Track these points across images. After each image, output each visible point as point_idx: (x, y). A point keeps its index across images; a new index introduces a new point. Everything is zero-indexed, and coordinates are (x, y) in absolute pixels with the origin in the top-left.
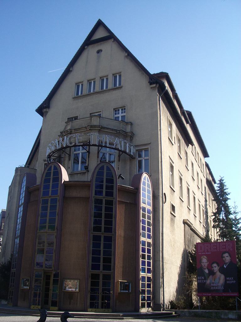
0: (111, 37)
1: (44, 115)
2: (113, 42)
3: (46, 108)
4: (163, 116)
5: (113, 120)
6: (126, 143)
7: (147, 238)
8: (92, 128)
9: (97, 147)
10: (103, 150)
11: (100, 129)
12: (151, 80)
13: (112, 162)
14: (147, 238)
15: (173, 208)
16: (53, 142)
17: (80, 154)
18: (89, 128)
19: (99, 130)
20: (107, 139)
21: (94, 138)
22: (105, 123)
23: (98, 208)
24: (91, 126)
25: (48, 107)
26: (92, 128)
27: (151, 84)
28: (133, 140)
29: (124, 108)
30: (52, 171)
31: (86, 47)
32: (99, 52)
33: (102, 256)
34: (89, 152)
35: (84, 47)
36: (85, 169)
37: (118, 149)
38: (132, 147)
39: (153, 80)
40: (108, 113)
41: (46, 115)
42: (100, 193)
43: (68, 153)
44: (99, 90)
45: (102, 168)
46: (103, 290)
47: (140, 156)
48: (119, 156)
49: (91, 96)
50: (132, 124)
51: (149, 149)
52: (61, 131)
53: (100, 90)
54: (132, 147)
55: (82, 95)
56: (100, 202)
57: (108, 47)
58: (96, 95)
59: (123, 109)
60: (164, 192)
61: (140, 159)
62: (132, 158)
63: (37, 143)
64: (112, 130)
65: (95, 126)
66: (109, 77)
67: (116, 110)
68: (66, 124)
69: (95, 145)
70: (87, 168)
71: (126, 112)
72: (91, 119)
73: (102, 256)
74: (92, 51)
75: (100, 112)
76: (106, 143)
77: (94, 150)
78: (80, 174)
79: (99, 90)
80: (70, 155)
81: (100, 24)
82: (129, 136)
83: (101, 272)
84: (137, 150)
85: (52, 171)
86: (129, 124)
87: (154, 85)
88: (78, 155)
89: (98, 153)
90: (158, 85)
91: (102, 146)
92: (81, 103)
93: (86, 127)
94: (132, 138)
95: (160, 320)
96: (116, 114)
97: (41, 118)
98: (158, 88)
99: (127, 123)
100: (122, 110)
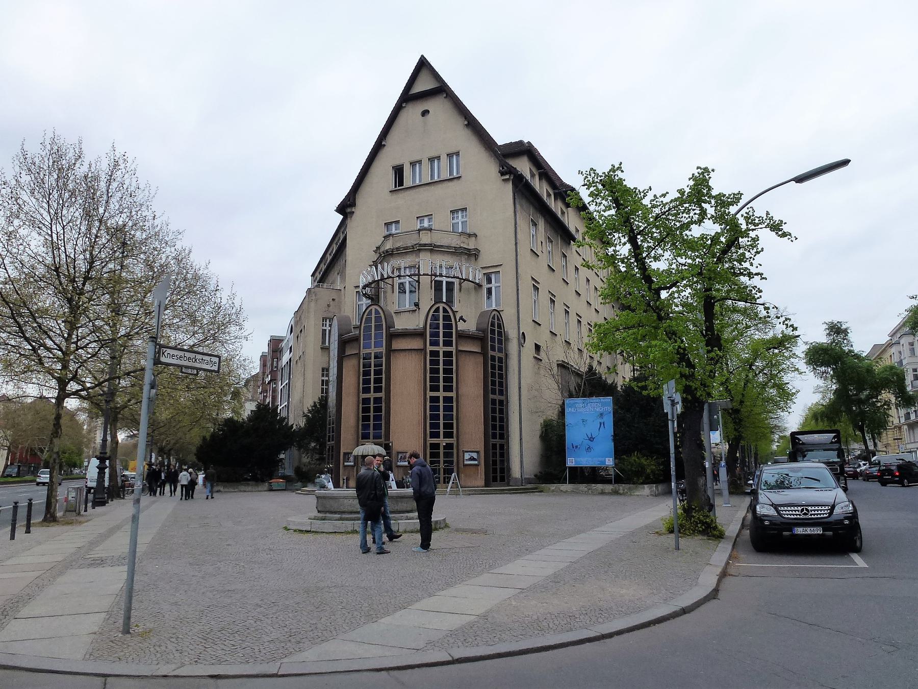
0: (442, 90)
6: (467, 268)
15: (538, 348)
23: (435, 362)
24: (421, 245)
25: (353, 204)
26: (418, 249)
29: (464, 210)
30: (373, 316)
32: (425, 113)
33: (441, 422)
34: (418, 281)
40: (442, 221)
42: (436, 343)
45: (437, 310)
47: (489, 281)
57: (437, 106)
61: (489, 286)
62: (479, 286)
63: (335, 248)
64: (448, 247)
65: (425, 245)
70: (417, 305)
73: (441, 422)
74: (412, 112)
81: (423, 65)
82: (472, 255)
83: (443, 441)
85: (373, 316)
92: (403, 199)
99: (470, 235)
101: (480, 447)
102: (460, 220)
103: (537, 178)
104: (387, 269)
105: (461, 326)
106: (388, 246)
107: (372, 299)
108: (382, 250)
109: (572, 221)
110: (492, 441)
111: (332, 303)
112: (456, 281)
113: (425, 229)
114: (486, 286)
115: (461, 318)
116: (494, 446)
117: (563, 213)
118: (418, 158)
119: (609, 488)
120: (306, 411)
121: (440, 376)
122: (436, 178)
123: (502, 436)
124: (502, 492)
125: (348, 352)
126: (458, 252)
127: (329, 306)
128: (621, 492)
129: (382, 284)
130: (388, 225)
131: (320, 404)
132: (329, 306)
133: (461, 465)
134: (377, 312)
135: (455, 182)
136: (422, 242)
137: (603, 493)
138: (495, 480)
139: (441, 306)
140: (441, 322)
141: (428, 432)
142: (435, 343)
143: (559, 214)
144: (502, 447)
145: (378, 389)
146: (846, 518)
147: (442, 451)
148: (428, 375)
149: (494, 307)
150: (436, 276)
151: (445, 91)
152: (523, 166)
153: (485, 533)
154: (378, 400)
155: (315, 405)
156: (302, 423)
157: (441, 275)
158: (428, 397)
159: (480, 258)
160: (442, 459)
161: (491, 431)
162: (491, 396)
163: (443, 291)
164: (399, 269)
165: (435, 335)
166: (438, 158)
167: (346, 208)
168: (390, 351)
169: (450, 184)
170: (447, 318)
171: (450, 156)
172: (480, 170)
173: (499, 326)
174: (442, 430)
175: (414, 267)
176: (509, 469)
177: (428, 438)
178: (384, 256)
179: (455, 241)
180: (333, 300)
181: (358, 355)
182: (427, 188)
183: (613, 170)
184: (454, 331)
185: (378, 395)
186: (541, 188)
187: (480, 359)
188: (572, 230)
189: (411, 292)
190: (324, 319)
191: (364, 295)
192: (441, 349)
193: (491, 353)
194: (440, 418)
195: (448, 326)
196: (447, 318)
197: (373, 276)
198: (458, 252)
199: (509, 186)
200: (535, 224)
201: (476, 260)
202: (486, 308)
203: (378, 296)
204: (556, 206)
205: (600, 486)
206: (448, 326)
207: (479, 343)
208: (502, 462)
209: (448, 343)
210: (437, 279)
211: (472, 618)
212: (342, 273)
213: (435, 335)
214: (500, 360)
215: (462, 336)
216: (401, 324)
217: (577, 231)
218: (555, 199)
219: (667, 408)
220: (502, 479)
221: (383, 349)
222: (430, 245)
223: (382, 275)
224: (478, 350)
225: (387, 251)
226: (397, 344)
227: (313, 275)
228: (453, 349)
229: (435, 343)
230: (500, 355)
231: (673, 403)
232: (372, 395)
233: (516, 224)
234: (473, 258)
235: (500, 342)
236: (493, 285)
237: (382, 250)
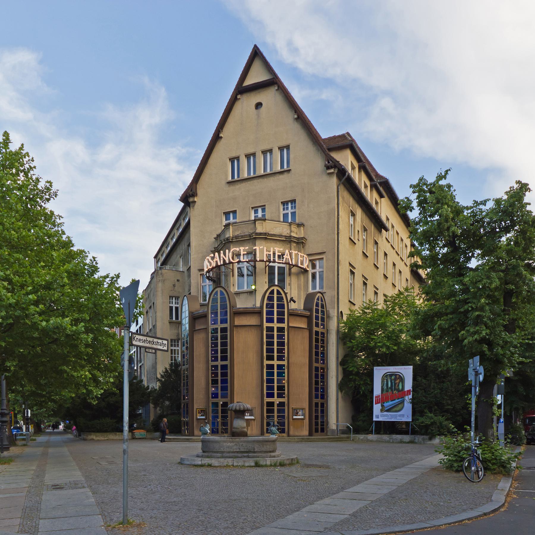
2: (276, 90)
12: (329, 162)
24: (257, 234)
25: (194, 195)
27: (328, 168)
29: (293, 201)
31: (239, 97)
32: (259, 105)
35: (236, 97)
37: (289, 264)
39: (331, 162)
41: (194, 206)
46: (278, 417)
47: (314, 267)
49: (252, 182)
52: (218, 234)
55: (239, 179)
56: (280, 358)
57: (269, 98)
60: (340, 311)
62: (305, 271)
64: (280, 236)
65: (261, 234)
74: (247, 103)
78: (245, 295)
87: (332, 171)
88: (242, 269)
90: (336, 171)
92: (239, 190)
95: (175, 435)
98: (337, 174)
101: (306, 405)
102: (290, 211)
103: (357, 170)
104: (228, 256)
105: (293, 306)
106: (230, 233)
107: (214, 281)
108: (222, 238)
109: (385, 209)
110: (315, 401)
111: (177, 283)
112: (287, 267)
113: (260, 219)
114: (310, 270)
115: (292, 299)
116: (317, 404)
117: (377, 203)
118: (251, 151)
119: (406, 438)
120: (159, 376)
121: (274, 347)
122: (268, 171)
123: (323, 397)
124: (323, 440)
126: (288, 240)
127: (174, 286)
128: (416, 441)
129: (223, 269)
130: (227, 214)
131: (171, 369)
132: (174, 286)
133: (291, 420)
134: (222, 293)
135: (286, 175)
136: (257, 231)
137: (401, 442)
138: (317, 431)
139: (275, 289)
140: (275, 303)
143: (374, 206)
144: (322, 405)
145: (224, 358)
146: (239, 99)
147: (276, 408)
148: (265, 347)
149: (318, 289)
150: (270, 262)
151: (276, 83)
152: (346, 159)
153: (328, 467)
155: (166, 371)
156: (157, 386)
157: (274, 262)
158: (265, 365)
159: (307, 246)
160: (276, 414)
161: (314, 393)
163: (278, 276)
164: (238, 255)
165: (270, 313)
166: (271, 151)
167: (188, 198)
169: (281, 176)
170: (280, 299)
171: (281, 149)
172: (306, 160)
173: (322, 306)
174: (276, 392)
175: (251, 253)
176: (327, 423)
177: (265, 398)
178: (222, 243)
180: (178, 280)
181: (206, 329)
182: (261, 180)
183: (440, 177)
184: (286, 310)
185: (224, 363)
186: (360, 180)
187: (307, 334)
188: (384, 219)
189: (248, 275)
190: (171, 297)
191: (208, 278)
192: (275, 325)
193: (315, 329)
194: (273, 383)
195: (281, 306)
196: (280, 299)
197: (217, 262)
198: (288, 240)
199: (334, 180)
200: (353, 215)
202: (310, 290)
203: (219, 279)
204: (371, 196)
205: (399, 437)
206: (281, 306)
207: (305, 320)
208: (322, 417)
210: (271, 264)
211: (346, 516)
212: (186, 257)
213: (270, 313)
214: (323, 333)
215: (293, 314)
216: (241, 304)
217: (388, 219)
218: (371, 190)
219: (471, 377)
220: (323, 430)
222: (265, 234)
223: (224, 261)
224: (304, 326)
225: (228, 239)
227: (155, 257)
228: (285, 325)
230: (323, 331)
231: (477, 374)
235: (323, 319)
237: (222, 238)
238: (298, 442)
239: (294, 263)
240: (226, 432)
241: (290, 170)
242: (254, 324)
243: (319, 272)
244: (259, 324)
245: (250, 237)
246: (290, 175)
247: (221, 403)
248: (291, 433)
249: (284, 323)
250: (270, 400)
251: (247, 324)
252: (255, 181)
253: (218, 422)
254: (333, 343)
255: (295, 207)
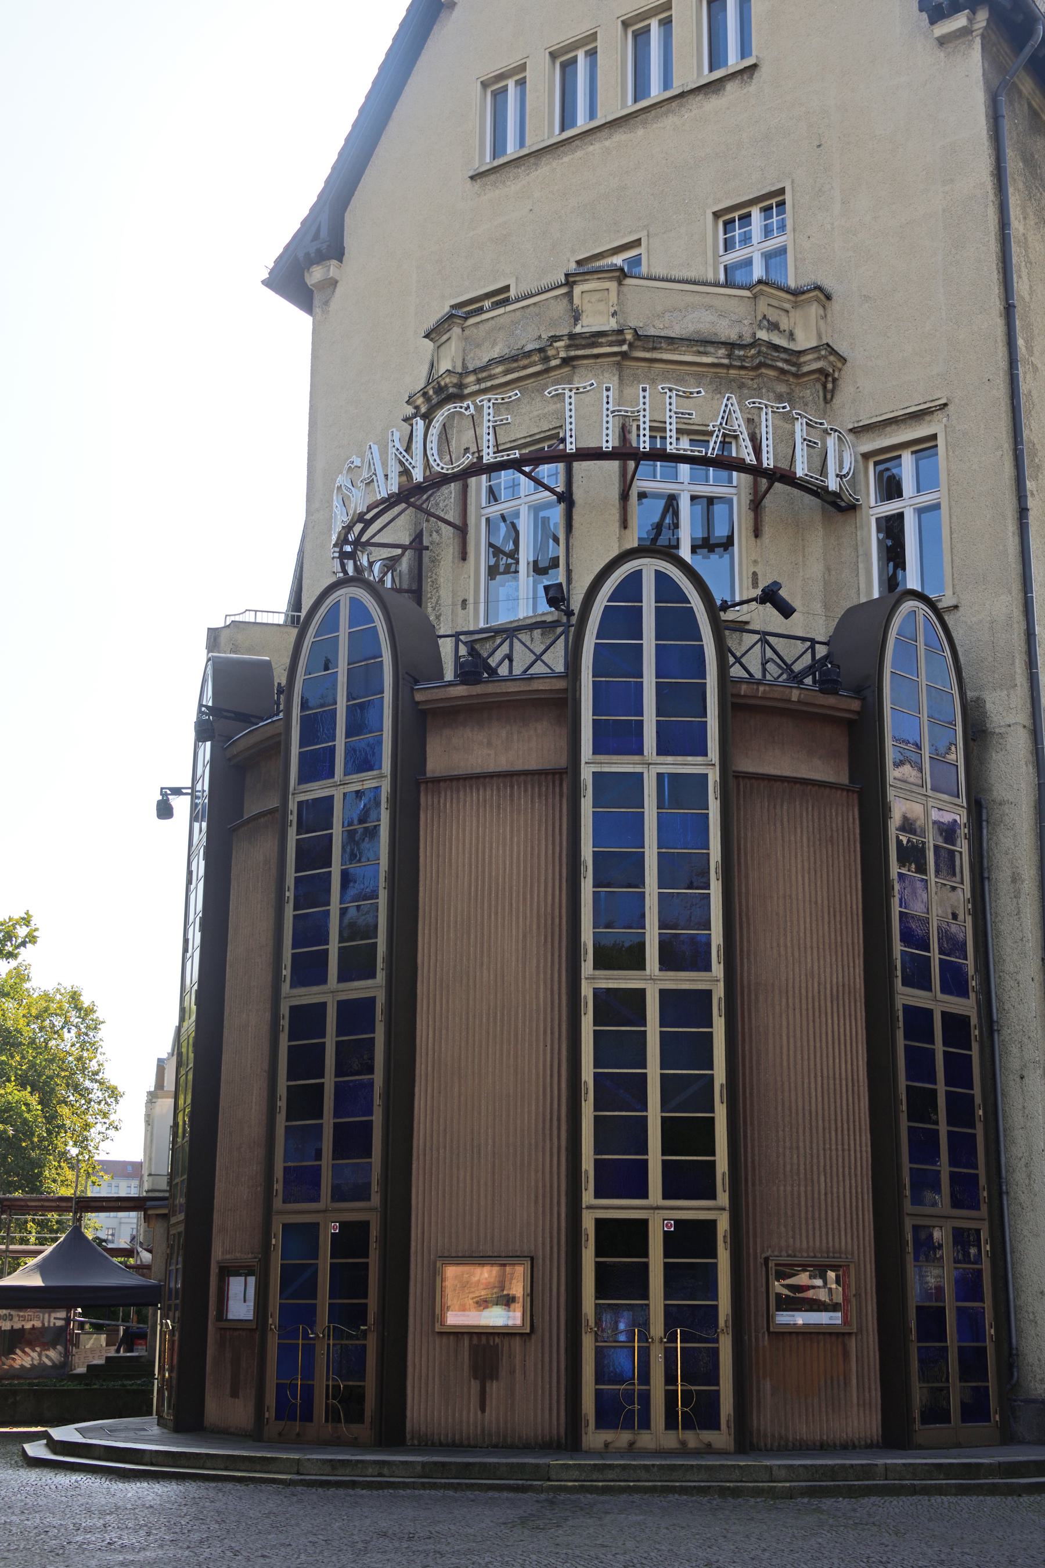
1: (316, 302)
3: (321, 257)
4: (1032, 220)
5: (716, 284)
7: (943, 991)
8: (579, 350)
9: (614, 465)
10: (652, 481)
11: (625, 348)
13: (719, 545)
14: (943, 991)
16: (358, 462)
17: (524, 511)
18: (562, 354)
19: (624, 355)
20: (661, 405)
21: (590, 409)
22: (647, 309)
25: (336, 251)
26: (579, 350)
27: (937, 15)
28: (838, 400)
29: (773, 202)
34: (566, 498)
36: (552, 602)
37: (740, 466)
38: (831, 442)
40: (683, 247)
41: (326, 303)
43: (450, 517)
44: (624, 104)
47: (891, 489)
48: (756, 505)
49: (579, 154)
50: (828, 297)
51: (941, 441)
53: (707, 77)
54: (831, 442)
55: (525, 151)
58: (607, 143)
59: (770, 208)
61: (891, 508)
62: (839, 506)
65: (595, 337)
66: (528, 74)
67: (732, 218)
68: (429, 344)
69: (596, 455)
71: (789, 224)
72: (570, 295)
75: (637, 243)
76: (658, 429)
77: (597, 481)
79: (624, 104)
80: (462, 530)
82: (816, 376)
84: (866, 456)
86: (808, 301)
87: (960, 21)
89: (624, 496)
91: (639, 457)
93: (541, 350)
94: (835, 380)
96: (728, 245)
97: (296, 325)
98: (983, 36)
100: (767, 210)
125: (252, 809)
138: (936, 1414)
141: (588, 1164)
142: (620, 737)
154: (358, 1015)
159: (845, 393)
162: (906, 996)
168: (413, 785)
179: (728, 318)
182: (620, 137)
199: (971, 67)
201: (828, 397)
209: (680, 739)
220: (975, 1410)
221: (380, 780)
226: (450, 753)
229: (620, 737)
232: (332, 991)
233: (1004, 224)
234: (810, 392)
236: (907, 505)
238: (790, 1494)
239: (768, 461)
240: (356, 1416)
241: (754, 67)
242: (533, 765)
243: (920, 511)
244: (563, 762)
245: (546, 359)
246: (753, 88)
247: (334, 1228)
248: (766, 1421)
249: (702, 750)
250: (622, 1209)
251: (492, 768)
252: (595, 147)
253: (310, 1350)
254: (1015, 879)
255: (782, 227)
